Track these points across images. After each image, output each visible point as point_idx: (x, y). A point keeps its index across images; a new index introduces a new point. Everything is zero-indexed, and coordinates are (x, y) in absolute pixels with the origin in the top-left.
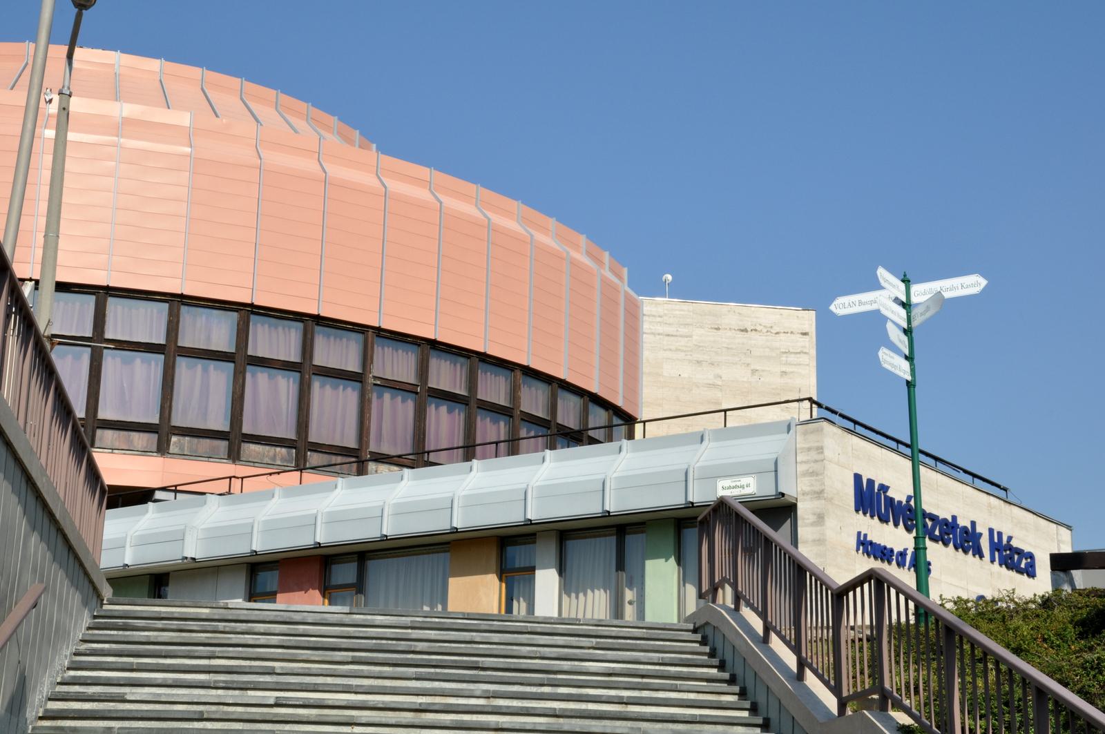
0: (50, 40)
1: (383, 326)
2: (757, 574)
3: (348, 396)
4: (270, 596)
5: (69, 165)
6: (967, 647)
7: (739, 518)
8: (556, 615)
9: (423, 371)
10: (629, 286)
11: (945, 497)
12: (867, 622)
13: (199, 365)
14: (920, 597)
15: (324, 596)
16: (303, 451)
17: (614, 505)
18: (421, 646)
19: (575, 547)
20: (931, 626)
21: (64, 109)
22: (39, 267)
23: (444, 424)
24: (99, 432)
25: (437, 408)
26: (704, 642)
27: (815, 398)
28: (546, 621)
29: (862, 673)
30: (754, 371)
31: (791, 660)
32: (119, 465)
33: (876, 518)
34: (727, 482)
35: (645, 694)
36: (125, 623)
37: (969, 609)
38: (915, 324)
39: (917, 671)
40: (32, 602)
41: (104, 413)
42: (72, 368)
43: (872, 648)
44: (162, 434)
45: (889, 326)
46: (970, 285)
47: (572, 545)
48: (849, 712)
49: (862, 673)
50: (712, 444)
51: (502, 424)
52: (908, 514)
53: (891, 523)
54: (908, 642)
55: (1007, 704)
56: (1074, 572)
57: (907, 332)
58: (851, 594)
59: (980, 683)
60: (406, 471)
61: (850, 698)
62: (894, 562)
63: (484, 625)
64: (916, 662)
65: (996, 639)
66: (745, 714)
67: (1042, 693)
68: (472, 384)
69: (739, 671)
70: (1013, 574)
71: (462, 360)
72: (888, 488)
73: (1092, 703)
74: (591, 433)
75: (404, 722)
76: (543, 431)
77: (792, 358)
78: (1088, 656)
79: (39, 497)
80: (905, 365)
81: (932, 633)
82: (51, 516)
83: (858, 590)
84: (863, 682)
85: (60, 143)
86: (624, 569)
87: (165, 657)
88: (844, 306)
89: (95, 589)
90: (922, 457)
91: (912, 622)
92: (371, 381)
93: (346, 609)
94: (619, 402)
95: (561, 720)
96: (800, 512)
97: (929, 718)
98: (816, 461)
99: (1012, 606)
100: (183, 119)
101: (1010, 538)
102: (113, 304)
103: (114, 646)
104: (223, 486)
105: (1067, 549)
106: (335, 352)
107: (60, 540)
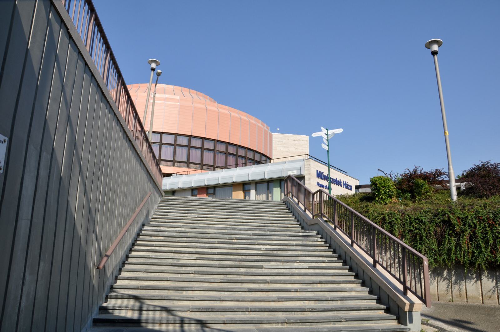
0: (152, 83)
1: (219, 140)
2: (296, 190)
3: (211, 154)
4: (196, 195)
5: (155, 107)
6: (338, 204)
7: (293, 179)
8: (255, 199)
9: (227, 149)
10: (270, 131)
11: (335, 174)
12: (319, 200)
13: (181, 148)
14: (329, 195)
15: (207, 196)
16: (202, 166)
17: (267, 177)
18: (227, 206)
19: (259, 186)
20: (331, 200)
21: (154, 96)
22: (149, 128)
23: (231, 160)
24: (161, 162)
25: (230, 157)
26: (285, 204)
27: (309, 154)
28: (253, 200)
29: (317, 210)
30: (296, 149)
31: (303, 208)
32: (166, 169)
33: (321, 179)
34: (290, 172)
35: (273, 215)
36: (167, 200)
37: (339, 197)
38: (329, 139)
39: (328, 209)
40: (149, 196)
41: (162, 158)
42: (156, 148)
43: (319, 205)
44: (174, 162)
45: (324, 139)
46: (340, 131)
47: (258, 185)
48: (315, 218)
49: (317, 210)
50: (287, 164)
51: (243, 160)
52: (327, 178)
53: (324, 180)
54: (327, 204)
55: (345, 215)
56: (359, 189)
57: (327, 140)
58: (316, 194)
59: (341, 211)
60: (223, 170)
61: (315, 215)
62: (324, 188)
63: (240, 201)
64: (328, 208)
65: (344, 203)
66: (294, 219)
67: (352, 213)
68: (237, 151)
69: (293, 210)
70: (348, 190)
71: (235, 146)
72: (323, 173)
73: (362, 214)
74: (262, 162)
75: (224, 221)
76: (252, 161)
77: (304, 146)
78: (361, 205)
79: (150, 175)
80: (327, 147)
81: (332, 202)
82: (152, 178)
83: (317, 193)
84: (318, 212)
85: (154, 103)
86: (269, 190)
87: (175, 207)
88: (315, 135)
89: (161, 193)
90: (330, 166)
91: (328, 200)
92: (216, 151)
93: (211, 198)
94: (268, 155)
95: (256, 221)
96: (305, 178)
97: (330, 219)
98: (309, 167)
99: (347, 196)
100: (177, 97)
101: (347, 183)
102: (164, 136)
103: (165, 205)
104: (186, 173)
105: (358, 184)
106: (208, 145)
107: (154, 183)
